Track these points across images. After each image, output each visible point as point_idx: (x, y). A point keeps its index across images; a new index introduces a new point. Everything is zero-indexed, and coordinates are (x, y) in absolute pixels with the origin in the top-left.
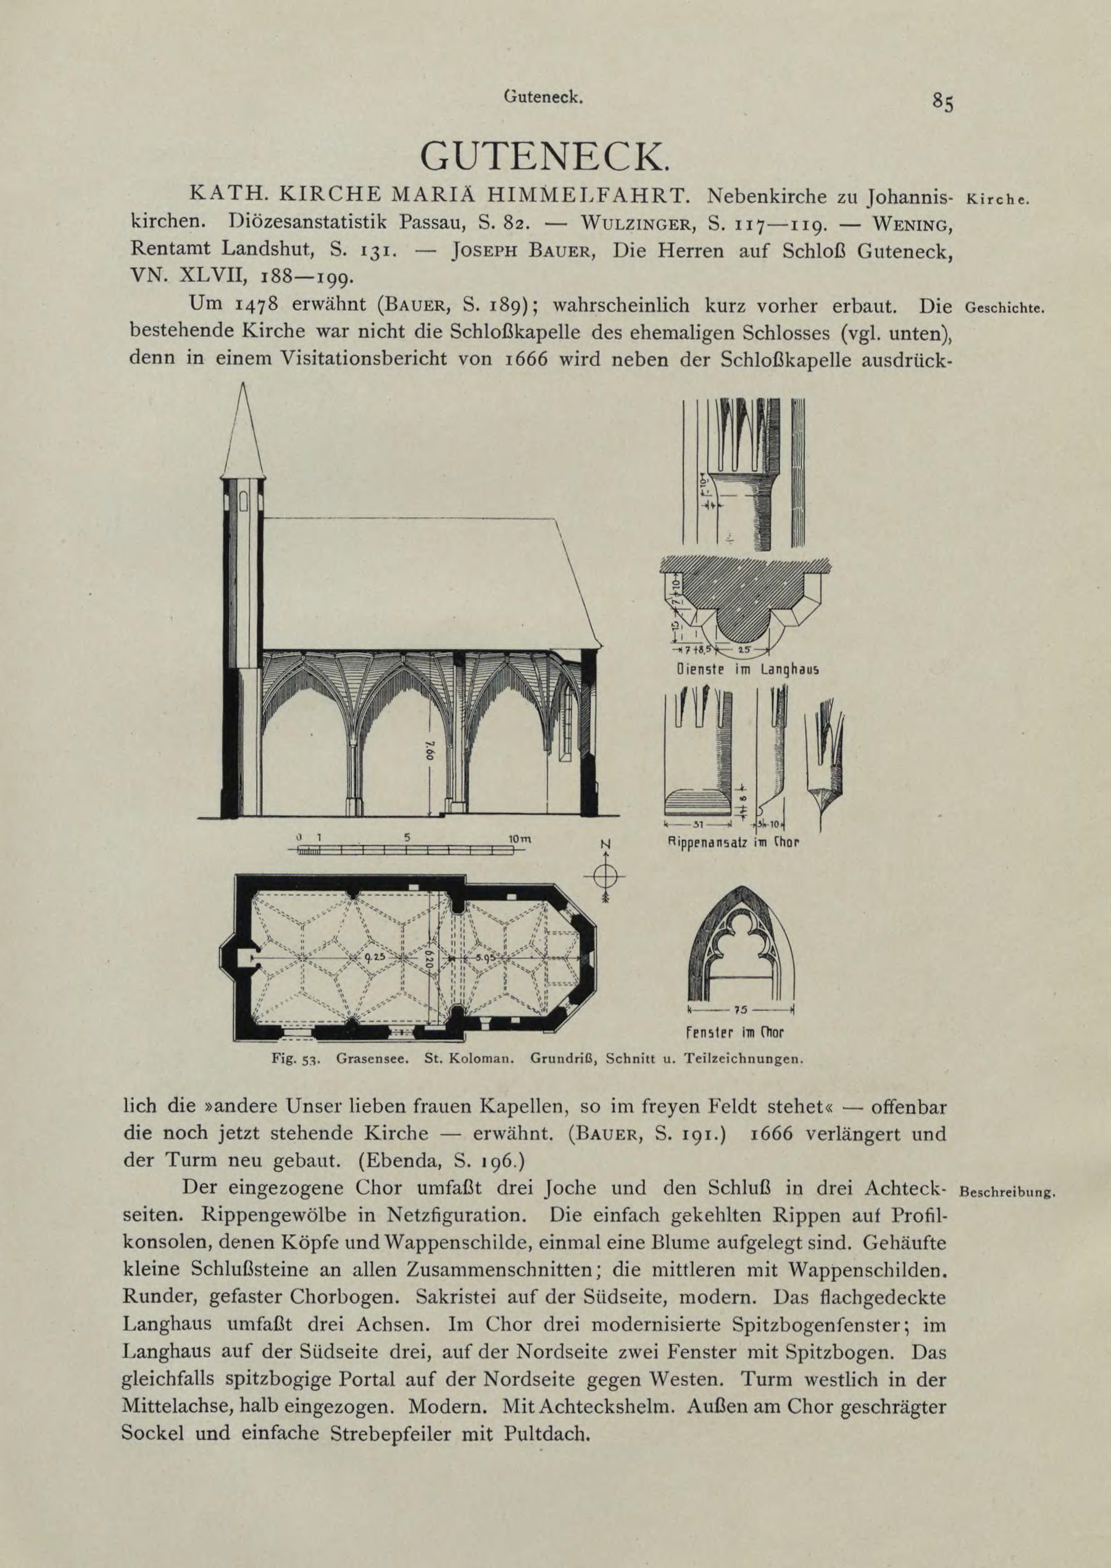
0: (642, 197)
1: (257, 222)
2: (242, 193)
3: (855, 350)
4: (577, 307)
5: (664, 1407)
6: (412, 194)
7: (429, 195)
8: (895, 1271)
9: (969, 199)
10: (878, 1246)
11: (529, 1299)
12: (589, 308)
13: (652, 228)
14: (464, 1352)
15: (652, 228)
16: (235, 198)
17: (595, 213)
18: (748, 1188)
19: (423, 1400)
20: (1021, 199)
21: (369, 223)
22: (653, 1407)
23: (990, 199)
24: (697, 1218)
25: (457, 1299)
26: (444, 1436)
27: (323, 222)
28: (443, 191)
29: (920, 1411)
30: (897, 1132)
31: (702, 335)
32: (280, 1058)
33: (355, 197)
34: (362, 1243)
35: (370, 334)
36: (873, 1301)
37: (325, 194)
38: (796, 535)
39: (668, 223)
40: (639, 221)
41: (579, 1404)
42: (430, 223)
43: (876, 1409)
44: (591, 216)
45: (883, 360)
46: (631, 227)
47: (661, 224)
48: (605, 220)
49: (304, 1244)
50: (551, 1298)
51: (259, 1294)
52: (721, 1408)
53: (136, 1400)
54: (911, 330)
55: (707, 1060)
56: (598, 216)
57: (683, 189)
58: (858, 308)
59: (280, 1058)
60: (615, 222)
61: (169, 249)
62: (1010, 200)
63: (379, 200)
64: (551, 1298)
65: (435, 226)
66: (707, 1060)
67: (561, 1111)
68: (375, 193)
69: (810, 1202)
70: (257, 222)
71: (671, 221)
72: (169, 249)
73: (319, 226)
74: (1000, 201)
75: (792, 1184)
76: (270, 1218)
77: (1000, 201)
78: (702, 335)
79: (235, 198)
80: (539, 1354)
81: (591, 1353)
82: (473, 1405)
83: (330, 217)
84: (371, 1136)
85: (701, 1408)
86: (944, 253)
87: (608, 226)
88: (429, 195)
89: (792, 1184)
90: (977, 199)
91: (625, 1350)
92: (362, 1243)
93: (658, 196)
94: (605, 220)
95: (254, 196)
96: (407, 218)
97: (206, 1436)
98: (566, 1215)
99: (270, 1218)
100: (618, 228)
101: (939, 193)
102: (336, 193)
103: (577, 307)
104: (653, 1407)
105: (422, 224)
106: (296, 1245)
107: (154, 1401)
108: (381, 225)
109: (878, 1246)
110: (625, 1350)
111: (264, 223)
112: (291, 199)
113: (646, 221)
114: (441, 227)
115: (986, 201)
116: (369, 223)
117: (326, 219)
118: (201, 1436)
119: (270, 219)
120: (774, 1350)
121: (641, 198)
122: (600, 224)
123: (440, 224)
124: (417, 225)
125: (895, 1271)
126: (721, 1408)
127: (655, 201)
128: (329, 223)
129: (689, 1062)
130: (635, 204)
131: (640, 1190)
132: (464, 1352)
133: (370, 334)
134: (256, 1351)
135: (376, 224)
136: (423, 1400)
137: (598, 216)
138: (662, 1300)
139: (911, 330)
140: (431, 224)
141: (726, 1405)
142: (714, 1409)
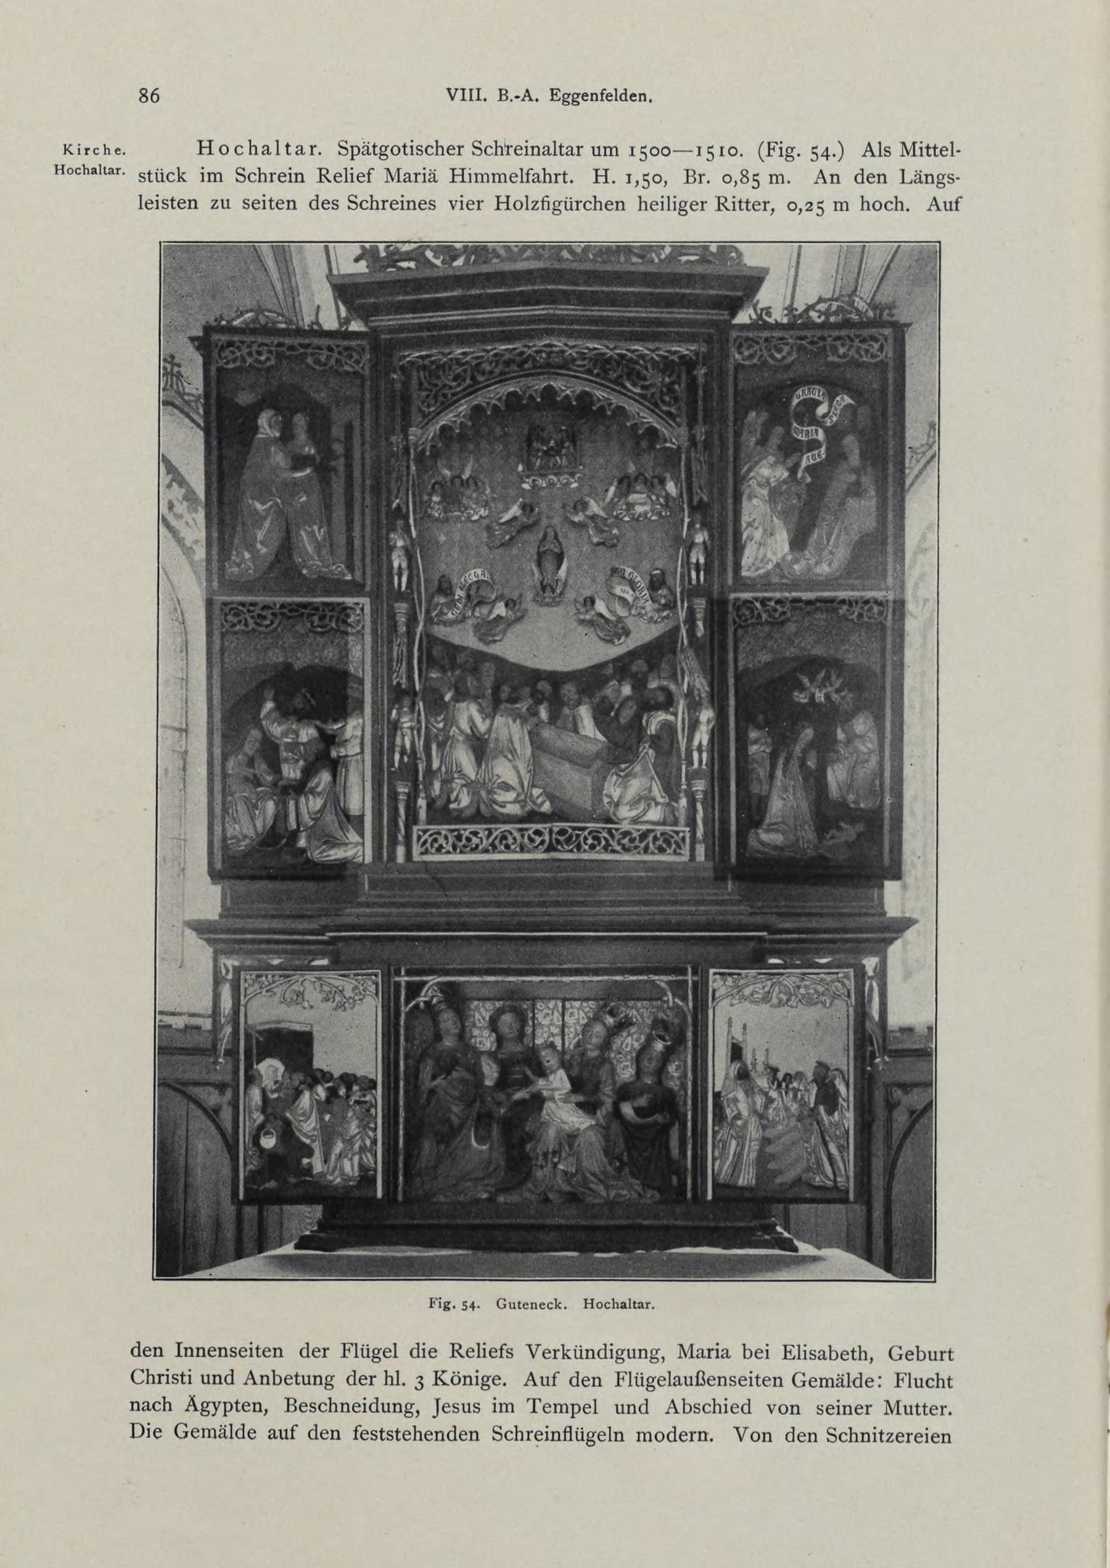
5: (780, 178)
10: (807, 1384)
11: (551, 1382)
12: (157, 1380)
18: (913, 1382)
19: (898, 1402)
20: (117, 150)
22: (613, 1436)
25: (164, 1379)
29: (562, 207)
31: (480, 1381)
36: (655, 1384)
41: (237, 1403)
43: (323, 1408)
49: (456, 1380)
52: (701, 1381)
53: (914, 144)
78: (480, 1381)
81: (754, 1380)
82: (700, 1433)
84: (439, 1382)
85: (941, 206)
93: (438, 1379)
97: (211, 1380)
104: (613, 1436)
106: (448, 1381)
107: (932, 145)
109: (807, 1384)
118: (206, 1381)
126: (701, 1381)
134: (563, 1380)
136: (898, 1402)
138: (502, 1382)
141: (706, 1378)
142: (694, 1382)
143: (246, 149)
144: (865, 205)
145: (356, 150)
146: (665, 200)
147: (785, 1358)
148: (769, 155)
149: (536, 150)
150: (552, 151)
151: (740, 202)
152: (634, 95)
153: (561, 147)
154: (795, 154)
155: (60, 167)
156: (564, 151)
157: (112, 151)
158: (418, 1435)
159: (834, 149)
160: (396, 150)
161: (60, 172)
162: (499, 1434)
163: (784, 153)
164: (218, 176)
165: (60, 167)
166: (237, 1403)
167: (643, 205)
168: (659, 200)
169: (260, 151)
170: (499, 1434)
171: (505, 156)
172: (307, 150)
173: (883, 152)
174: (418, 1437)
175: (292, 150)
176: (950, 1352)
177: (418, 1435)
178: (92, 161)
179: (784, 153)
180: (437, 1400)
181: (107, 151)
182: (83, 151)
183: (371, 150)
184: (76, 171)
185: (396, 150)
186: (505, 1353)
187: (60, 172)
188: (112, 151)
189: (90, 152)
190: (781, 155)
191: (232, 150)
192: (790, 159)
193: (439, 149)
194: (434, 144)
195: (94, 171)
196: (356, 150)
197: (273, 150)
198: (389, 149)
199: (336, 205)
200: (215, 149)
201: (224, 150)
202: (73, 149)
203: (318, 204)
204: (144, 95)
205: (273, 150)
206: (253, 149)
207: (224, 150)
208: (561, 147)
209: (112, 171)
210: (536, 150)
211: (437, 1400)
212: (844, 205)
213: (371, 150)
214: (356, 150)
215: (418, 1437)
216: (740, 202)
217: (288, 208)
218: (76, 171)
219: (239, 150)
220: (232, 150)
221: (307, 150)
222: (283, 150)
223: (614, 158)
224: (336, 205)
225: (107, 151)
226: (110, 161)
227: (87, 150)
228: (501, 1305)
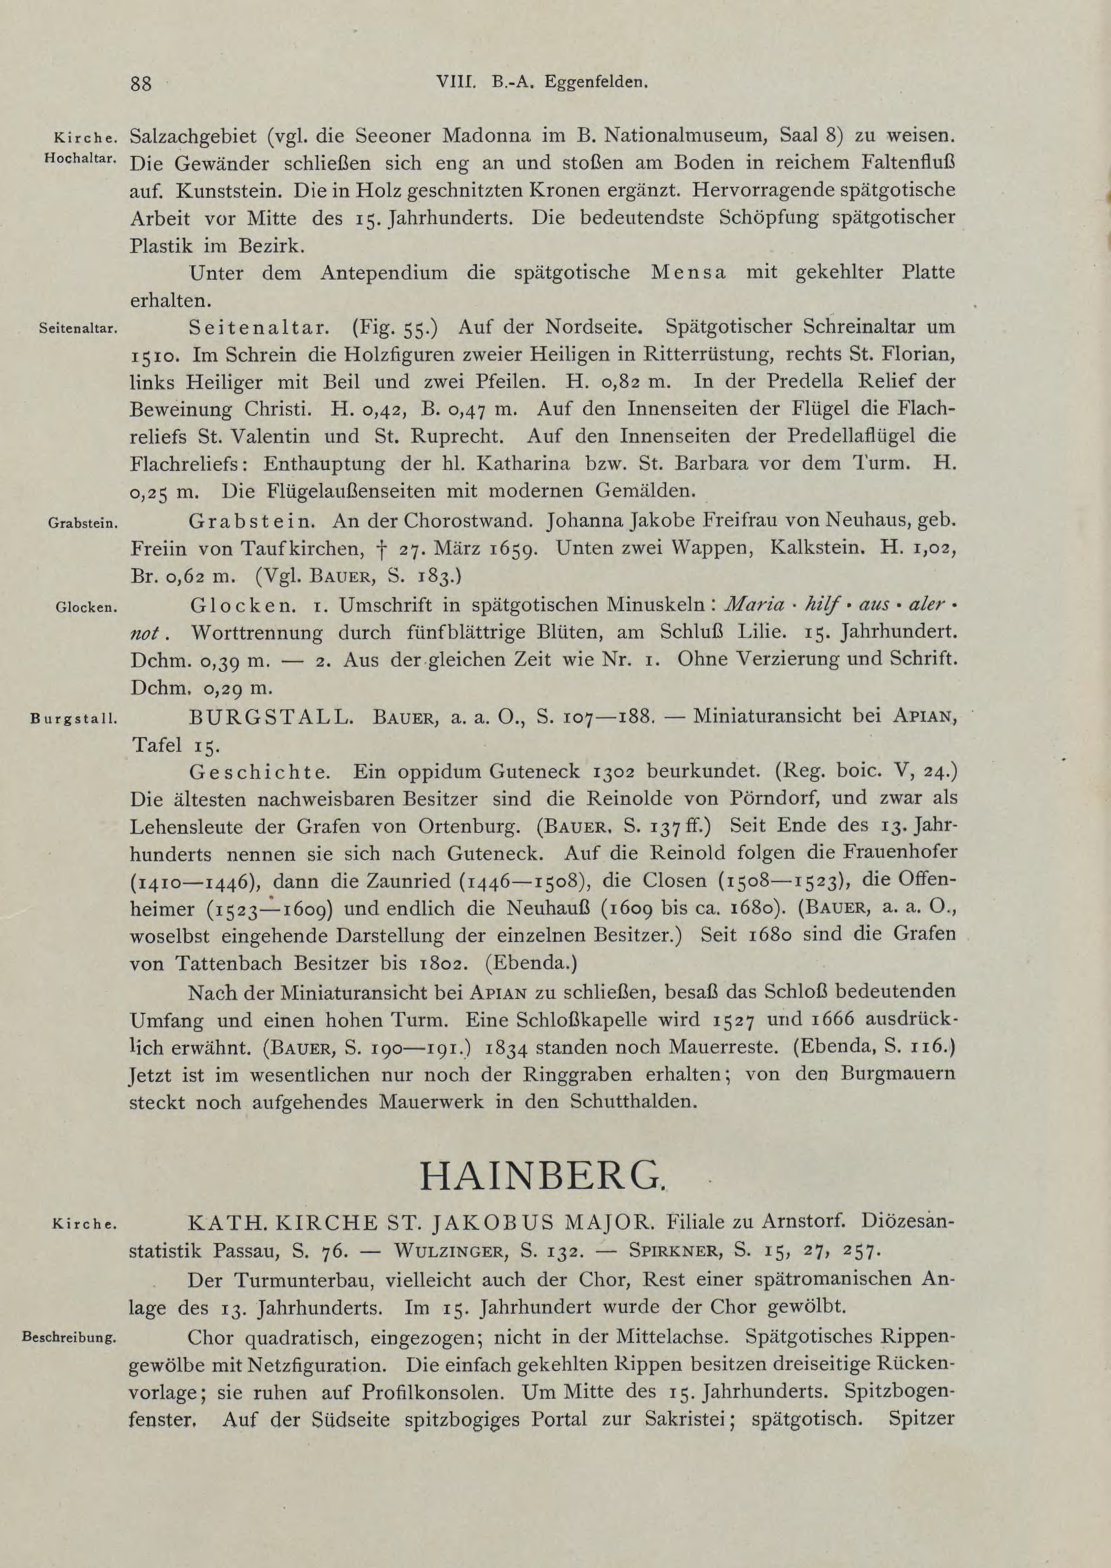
0: (354, 1225)
1: (891, 1222)
2: (241, 1224)
6: (586, 1222)
7: (461, 1223)
9: (55, 1224)
13: (465, 1255)
15: (465, 1255)
16: (234, 1228)
17: (408, 1241)
20: (108, 1224)
21: (183, 1253)
23: (77, 1223)
27: (137, 1252)
28: (645, 1218)
33: (351, 1226)
37: (321, 1223)
39: (482, 1251)
40: (452, 1248)
42: (244, 1251)
44: (405, 1244)
45: (887, 1018)
46: (444, 1255)
47: (475, 1251)
48: (418, 1248)
56: (412, 1244)
57: (415, 1216)
60: (428, 1250)
62: (97, 1225)
63: (376, 1229)
65: (249, 1255)
67: (745, 552)
68: (372, 1222)
70: (891, 1222)
71: (485, 1248)
73: (802, 1225)
74: (87, 1225)
77: (87, 1225)
79: (234, 1228)
80: (568, 328)
83: (144, 1247)
85: (358, 662)
86: (535, 855)
87: (421, 1254)
88: (461, 1223)
90: (63, 1223)
91: (469, 353)
92: (547, 1308)
94: (418, 1248)
95: (253, 1226)
96: (221, 1247)
98: (549, 218)
100: (431, 1256)
101: (678, 904)
102: (333, 1222)
105: (236, 1253)
108: (195, 1254)
110: (469, 353)
111: (898, 1223)
112: (200, 1228)
113: (459, 1248)
114: (255, 1256)
115: (73, 1226)
116: (183, 1253)
117: (140, 1249)
119: (903, 1219)
120: (304, 380)
121: (353, 1225)
122: (414, 1251)
123: (253, 1253)
124: (231, 1254)
127: (310, 1228)
128: (143, 1253)
130: (248, 1231)
135: (191, 1253)
137: (412, 1244)
140: (245, 1253)
145: (764, 1338)
146: (221, 378)
147: (469, 1025)
148: (363, 332)
149: (554, 464)
151: (644, 1334)
153: (893, 324)
154: (389, 331)
156: (896, 328)
157: (103, 1225)
159: (948, 769)
160: (896, 192)
163: (379, 330)
167: (331, 1021)
169: (81, 159)
172: (314, 329)
173: (949, 799)
175: (299, 329)
176: (588, 1304)
179: (379, 330)
183: (502, 606)
184: (67, 159)
185: (569, 274)
186: (229, 466)
188: (103, 1225)
189: (80, 1226)
190: (376, 332)
191: (233, 607)
196: (764, 1338)
197: (280, 328)
198: (717, 327)
199: (364, 1103)
200: (671, 274)
201: (226, 607)
205: (280, 328)
206: (255, 773)
207: (226, 607)
208: (893, 324)
210: (554, 464)
212: (425, 1308)
213: (502, 606)
214: (684, 328)
216: (644, 1334)
218: (67, 159)
219: (242, 774)
220: (233, 607)
221: (314, 329)
222: (226, 329)
223: (296, 281)
224: (364, 1103)
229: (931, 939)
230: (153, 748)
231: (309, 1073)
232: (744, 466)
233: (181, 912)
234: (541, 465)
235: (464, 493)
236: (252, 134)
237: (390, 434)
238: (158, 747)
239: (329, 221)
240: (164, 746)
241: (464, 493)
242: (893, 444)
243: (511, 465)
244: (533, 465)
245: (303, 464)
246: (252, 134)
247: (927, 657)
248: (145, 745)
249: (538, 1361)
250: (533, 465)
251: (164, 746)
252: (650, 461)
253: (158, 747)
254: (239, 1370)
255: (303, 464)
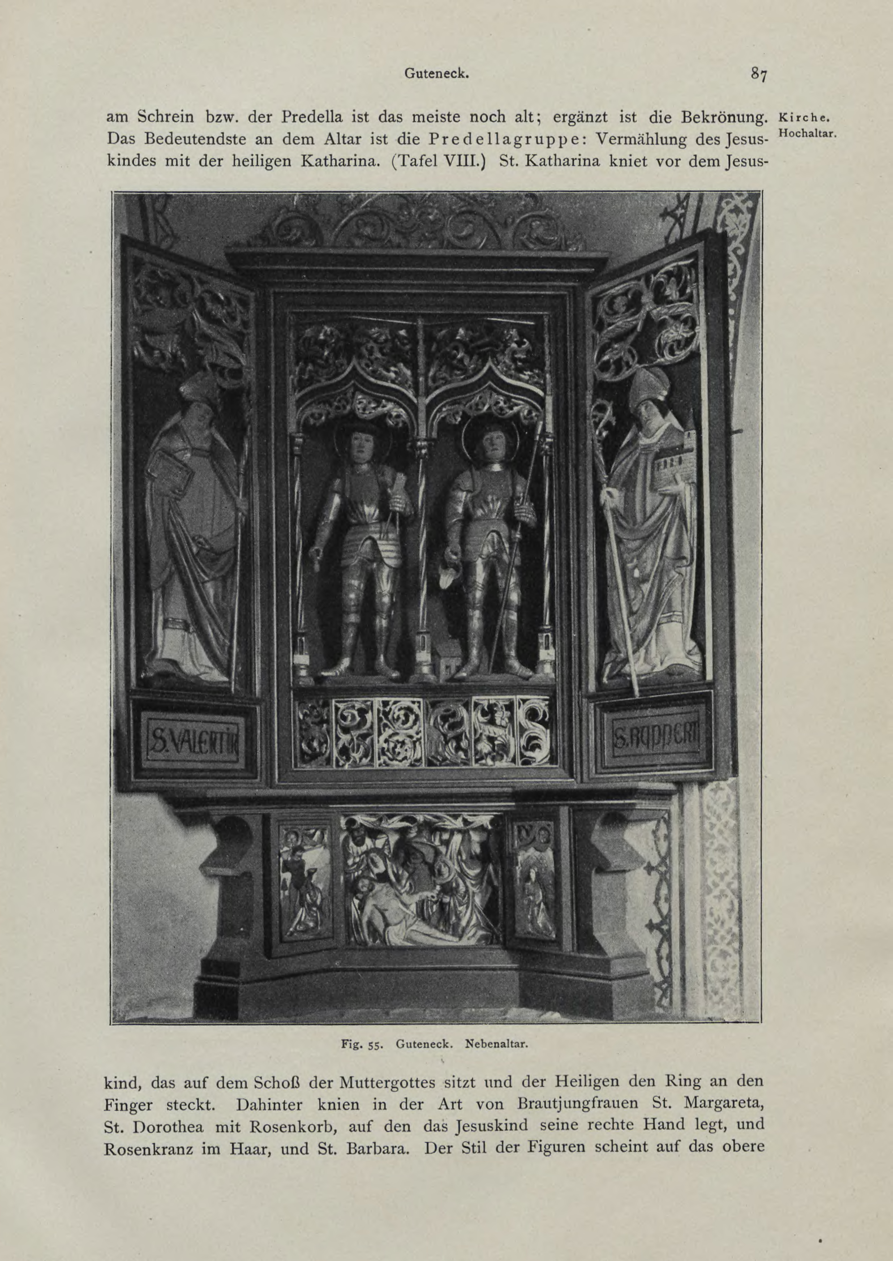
3: (407, 125)
4: (258, 1106)
8: (267, 1106)
14: (366, 1127)
24: (199, 1107)
26: (447, 1150)
30: (459, 1102)
32: (113, 1104)
34: (750, 1125)
35: (337, 1107)
38: (724, 503)
41: (622, 1123)
50: (313, 1084)
51: (175, 1103)
54: (281, 1102)
55: (583, 1083)
58: (378, 1150)
59: (113, 1104)
61: (282, 1106)
64: (313, 1084)
66: (583, 1083)
69: (732, 1092)
72: (282, 1106)
75: (377, 1101)
76: (692, 1083)
89: (377, 1101)
92: (750, 1125)
99: (692, 1083)
103: (258, 1106)
125: (267, 1106)
129: (294, 121)
131: (508, 1084)
132: (366, 1127)
133: (337, 1107)
139: (281, 1102)
143: (810, 118)
144: (237, 162)
150: (523, 118)
152: (432, 73)
153: (344, 137)
154: (763, 120)
155: (783, 131)
158: (182, 1127)
161: (783, 135)
162: (353, 1148)
164: (310, 140)
165: (783, 131)
166: (622, 1123)
167: (237, 162)
168: (250, 158)
170: (353, 1148)
171: (165, 123)
174: (182, 1129)
177: (182, 1127)
178: (810, 126)
180: (459, 1121)
181: (814, 118)
182: (795, 118)
187: (783, 135)
188: (818, 118)
192: (759, 124)
193: (315, 117)
194: (155, 113)
195: (812, 135)
199: (153, 162)
202: (787, 117)
203: (697, 162)
204: (755, 73)
208: (344, 137)
209: (825, 135)
211: (459, 1121)
212: (716, 162)
215: (182, 1129)
217: (285, 165)
218: (796, 134)
224: (153, 162)
225: (814, 118)
226: (822, 126)
227: (798, 117)
228: (400, 1045)
229: (421, 165)
230: (414, 164)
231: (550, 159)
232: (597, 163)
233: (246, 163)
234: (352, 162)
235: (179, 162)
236: (644, 159)
237: (511, 159)
238: (418, 162)
239: (145, 163)
240: (424, 162)
241: (179, 162)
242: (133, 1112)
243: (552, 162)
244: (571, 162)
245: (334, 162)
246: (644, 159)
247: (573, 160)
248: (408, 161)
249: (701, 114)
250: (346, 162)
251: (424, 162)
252: (508, 159)
253: (418, 162)
254: (187, 165)
255: (334, 162)
